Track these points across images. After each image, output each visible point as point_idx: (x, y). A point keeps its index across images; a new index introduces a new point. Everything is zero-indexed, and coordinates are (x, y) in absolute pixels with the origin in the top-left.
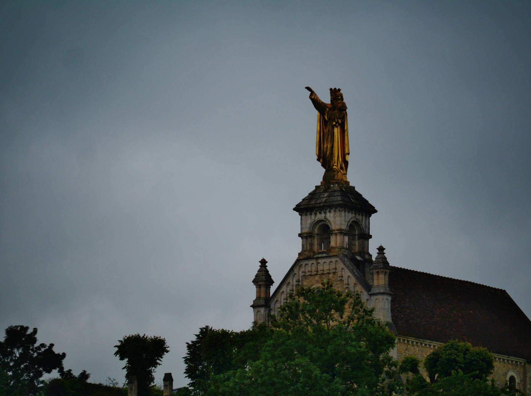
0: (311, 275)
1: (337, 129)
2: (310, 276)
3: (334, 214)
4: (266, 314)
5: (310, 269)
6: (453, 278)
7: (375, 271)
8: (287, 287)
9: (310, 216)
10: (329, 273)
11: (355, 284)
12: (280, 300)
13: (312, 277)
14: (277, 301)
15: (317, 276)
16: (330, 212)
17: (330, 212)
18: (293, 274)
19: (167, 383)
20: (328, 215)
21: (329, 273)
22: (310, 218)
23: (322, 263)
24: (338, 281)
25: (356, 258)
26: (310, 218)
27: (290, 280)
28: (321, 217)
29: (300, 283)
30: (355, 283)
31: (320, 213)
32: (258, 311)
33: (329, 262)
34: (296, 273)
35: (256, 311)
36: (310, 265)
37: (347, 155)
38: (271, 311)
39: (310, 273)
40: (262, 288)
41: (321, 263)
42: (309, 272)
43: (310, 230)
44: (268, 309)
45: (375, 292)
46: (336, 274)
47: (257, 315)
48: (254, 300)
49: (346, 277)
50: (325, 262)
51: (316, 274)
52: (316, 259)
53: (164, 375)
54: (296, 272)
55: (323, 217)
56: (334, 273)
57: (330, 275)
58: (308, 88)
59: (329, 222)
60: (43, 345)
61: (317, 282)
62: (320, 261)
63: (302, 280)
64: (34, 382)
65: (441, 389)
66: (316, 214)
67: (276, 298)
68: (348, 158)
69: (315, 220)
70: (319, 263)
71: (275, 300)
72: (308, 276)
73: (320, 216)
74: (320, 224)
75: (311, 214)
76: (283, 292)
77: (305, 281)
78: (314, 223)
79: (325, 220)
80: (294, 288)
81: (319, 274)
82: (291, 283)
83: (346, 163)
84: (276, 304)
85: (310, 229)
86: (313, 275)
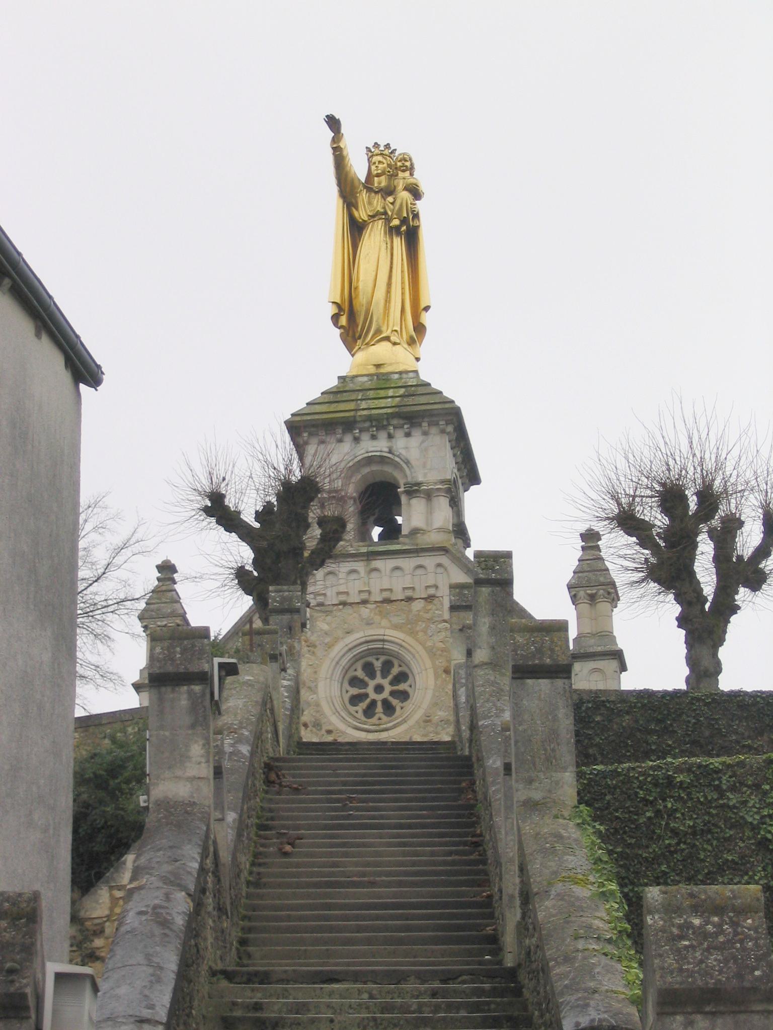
0: (344, 604)
1: (399, 239)
2: (341, 607)
3: (423, 442)
6: (720, 649)
7: (585, 591)
10: (409, 599)
13: (348, 610)
15: (368, 606)
37: (423, 313)
41: (382, 569)
46: (435, 602)
48: (142, 668)
51: (364, 602)
52: (365, 558)
53: (680, 629)
57: (414, 604)
58: (333, 123)
60: (400, 155)
61: (368, 624)
66: (357, 440)
68: (427, 319)
72: (336, 607)
73: (379, 446)
74: (375, 468)
83: (420, 329)
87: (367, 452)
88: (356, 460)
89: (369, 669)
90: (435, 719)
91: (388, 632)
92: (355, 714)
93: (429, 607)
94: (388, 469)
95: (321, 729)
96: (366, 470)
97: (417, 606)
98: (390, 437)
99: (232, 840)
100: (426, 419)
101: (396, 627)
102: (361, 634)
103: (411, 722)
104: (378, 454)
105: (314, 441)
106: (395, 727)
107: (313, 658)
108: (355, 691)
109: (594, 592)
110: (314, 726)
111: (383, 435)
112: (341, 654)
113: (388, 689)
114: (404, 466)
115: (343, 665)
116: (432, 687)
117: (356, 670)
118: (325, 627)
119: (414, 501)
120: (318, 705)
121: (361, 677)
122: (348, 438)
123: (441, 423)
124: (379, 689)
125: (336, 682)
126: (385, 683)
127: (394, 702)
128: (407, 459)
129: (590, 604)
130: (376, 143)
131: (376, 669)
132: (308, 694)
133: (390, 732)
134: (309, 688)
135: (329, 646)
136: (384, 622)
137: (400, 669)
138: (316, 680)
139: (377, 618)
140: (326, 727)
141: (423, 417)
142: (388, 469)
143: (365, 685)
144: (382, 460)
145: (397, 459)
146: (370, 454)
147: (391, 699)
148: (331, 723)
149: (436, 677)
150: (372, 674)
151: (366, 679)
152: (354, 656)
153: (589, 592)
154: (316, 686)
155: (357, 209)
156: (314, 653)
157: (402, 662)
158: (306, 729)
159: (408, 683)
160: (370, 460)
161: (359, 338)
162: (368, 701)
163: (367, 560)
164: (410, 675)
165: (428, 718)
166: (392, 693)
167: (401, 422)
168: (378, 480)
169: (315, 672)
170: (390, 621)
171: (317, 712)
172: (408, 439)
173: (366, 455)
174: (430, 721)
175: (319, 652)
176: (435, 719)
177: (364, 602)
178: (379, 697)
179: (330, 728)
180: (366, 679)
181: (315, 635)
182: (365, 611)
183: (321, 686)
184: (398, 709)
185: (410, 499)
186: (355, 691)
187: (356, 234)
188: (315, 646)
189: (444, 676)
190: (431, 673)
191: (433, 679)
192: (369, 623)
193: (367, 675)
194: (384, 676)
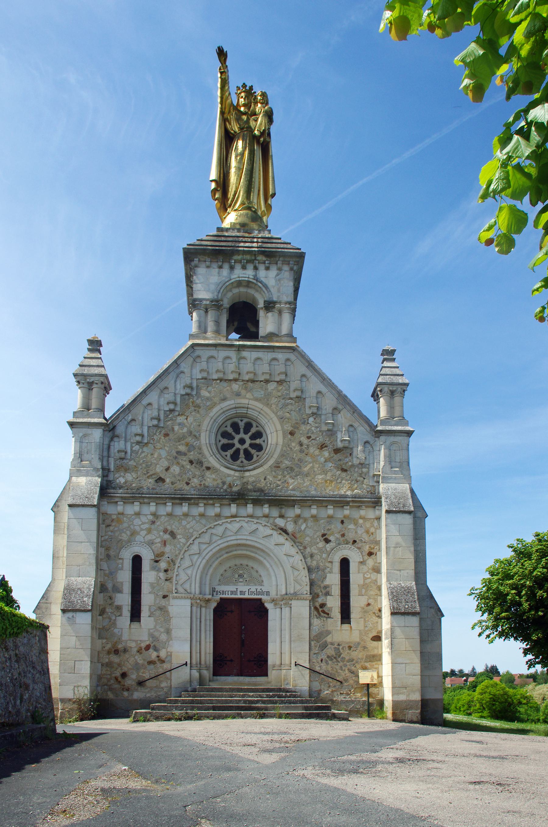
2: (218, 381)
3: (277, 275)
4: (105, 443)
5: (220, 366)
8: (160, 397)
9: (217, 270)
10: (267, 381)
11: (335, 409)
12: (140, 418)
13: (224, 384)
14: (133, 420)
15: (238, 383)
16: (267, 269)
17: (267, 269)
18: (178, 371)
19: (237, 702)
20: (262, 273)
21: (267, 381)
22: (219, 273)
23: (253, 359)
24: (291, 399)
25: (462, 89)
26: (217, 274)
27: (169, 382)
28: (244, 276)
29: (194, 393)
30: (334, 406)
31: (244, 268)
32: (85, 436)
33: (269, 359)
34: (185, 370)
35: (81, 434)
36: (220, 359)
38: (116, 439)
39: (221, 375)
40: (95, 390)
42: (218, 371)
43: (217, 296)
44: (109, 434)
45: (324, 493)
47: (81, 442)
49: (313, 393)
50: (258, 359)
51: (236, 380)
54: (185, 368)
55: (252, 277)
56: (280, 382)
58: (222, 54)
59: (264, 286)
62: (245, 354)
63: (197, 386)
64: (517, 716)
65: (524, 699)
66: (232, 268)
67: (130, 415)
69: (231, 280)
70: (244, 358)
71: (130, 418)
74: (242, 290)
75: (220, 267)
76: (150, 404)
77: (207, 389)
78: (228, 284)
79: (255, 281)
80: (178, 400)
81: (243, 381)
82: (171, 389)
84: (129, 426)
85: (218, 293)
86: (226, 380)
87: (239, 277)
88: (231, 282)
89: (235, 427)
90: (283, 466)
91: (251, 402)
92: (225, 457)
93: (280, 388)
94: (251, 291)
95: (202, 466)
96: (236, 291)
97: (272, 386)
98: (256, 268)
99: (473, 722)
100: (281, 259)
101: (256, 400)
102: (232, 402)
103: (266, 467)
104: (246, 279)
105: (203, 265)
106: (254, 469)
107: (198, 415)
108: (225, 441)
109: (394, 389)
110: (197, 464)
111: (250, 267)
112: (218, 414)
113: (248, 442)
114: (264, 289)
115: (238, 411)
116: (281, 444)
117: (226, 427)
118: (207, 394)
119: (270, 314)
120: (200, 449)
121: (230, 432)
122: (226, 266)
123: (291, 262)
124: (242, 442)
125: (213, 434)
126: (247, 437)
127: (253, 451)
128: (266, 285)
129: (390, 397)
130: (244, 84)
131: (240, 427)
132: (193, 440)
133: (251, 472)
134: (195, 436)
135: (211, 408)
136: (249, 395)
137: (257, 429)
138: (199, 431)
139: (243, 392)
140: (206, 465)
141: (280, 256)
142: (251, 291)
143: (233, 438)
144: (248, 284)
145: (260, 284)
146: (241, 279)
147: (250, 449)
148: (209, 462)
149: (284, 438)
150: (237, 431)
151: (233, 434)
152: (226, 417)
153: (391, 388)
154: (200, 435)
155: (230, 124)
156: (198, 411)
157: (259, 424)
158: (192, 465)
159: (262, 439)
160: (239, 284)
161: (230, 206)
162: (234, 449)
163: (238, 350)
164: (264, 434)
165: (277, 465)
166: (251, 445)
167: (264, 259)
168: (243, 299)
169: (199, 425)
170: (253, 395)
171: (200, 454)
172: (268, 271)
173: (238, 279)
174: (279, 467)
175: (202, 411)
176: (283, 466)
177: (236, 380)
178: (242, 447)
179: (209, 465)
180: (233, 434)
181: (200, 400)
182: (235, 387)
183: (203, 435)
184: (255, 457)
185: (267, 313)
186: (225, 441)
187: (229, 145)
188: (199, 407)
189: (289, 436)
190: (280, 433)
191: (282, 438)
192: (238, 395)
193: (234, 431)
194: (246, 433)
